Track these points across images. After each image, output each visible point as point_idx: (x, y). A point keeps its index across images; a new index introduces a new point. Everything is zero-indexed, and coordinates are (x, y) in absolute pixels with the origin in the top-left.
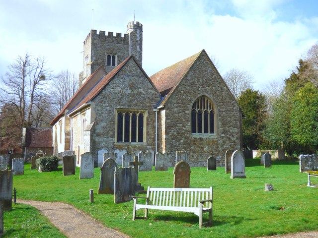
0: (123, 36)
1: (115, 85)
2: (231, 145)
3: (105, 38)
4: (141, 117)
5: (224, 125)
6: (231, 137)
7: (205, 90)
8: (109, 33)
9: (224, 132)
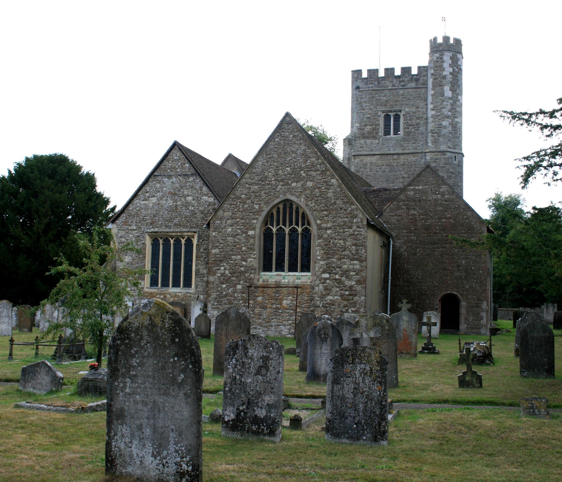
0: (414, 71)
1: (147, 194)
2: (342, 296)
3: (379, 83)
4: (189, 242)
5: (328, 255)
6: (344, 279)
7: (291, 190)
8: (387, 70)
9: (329, 269)
